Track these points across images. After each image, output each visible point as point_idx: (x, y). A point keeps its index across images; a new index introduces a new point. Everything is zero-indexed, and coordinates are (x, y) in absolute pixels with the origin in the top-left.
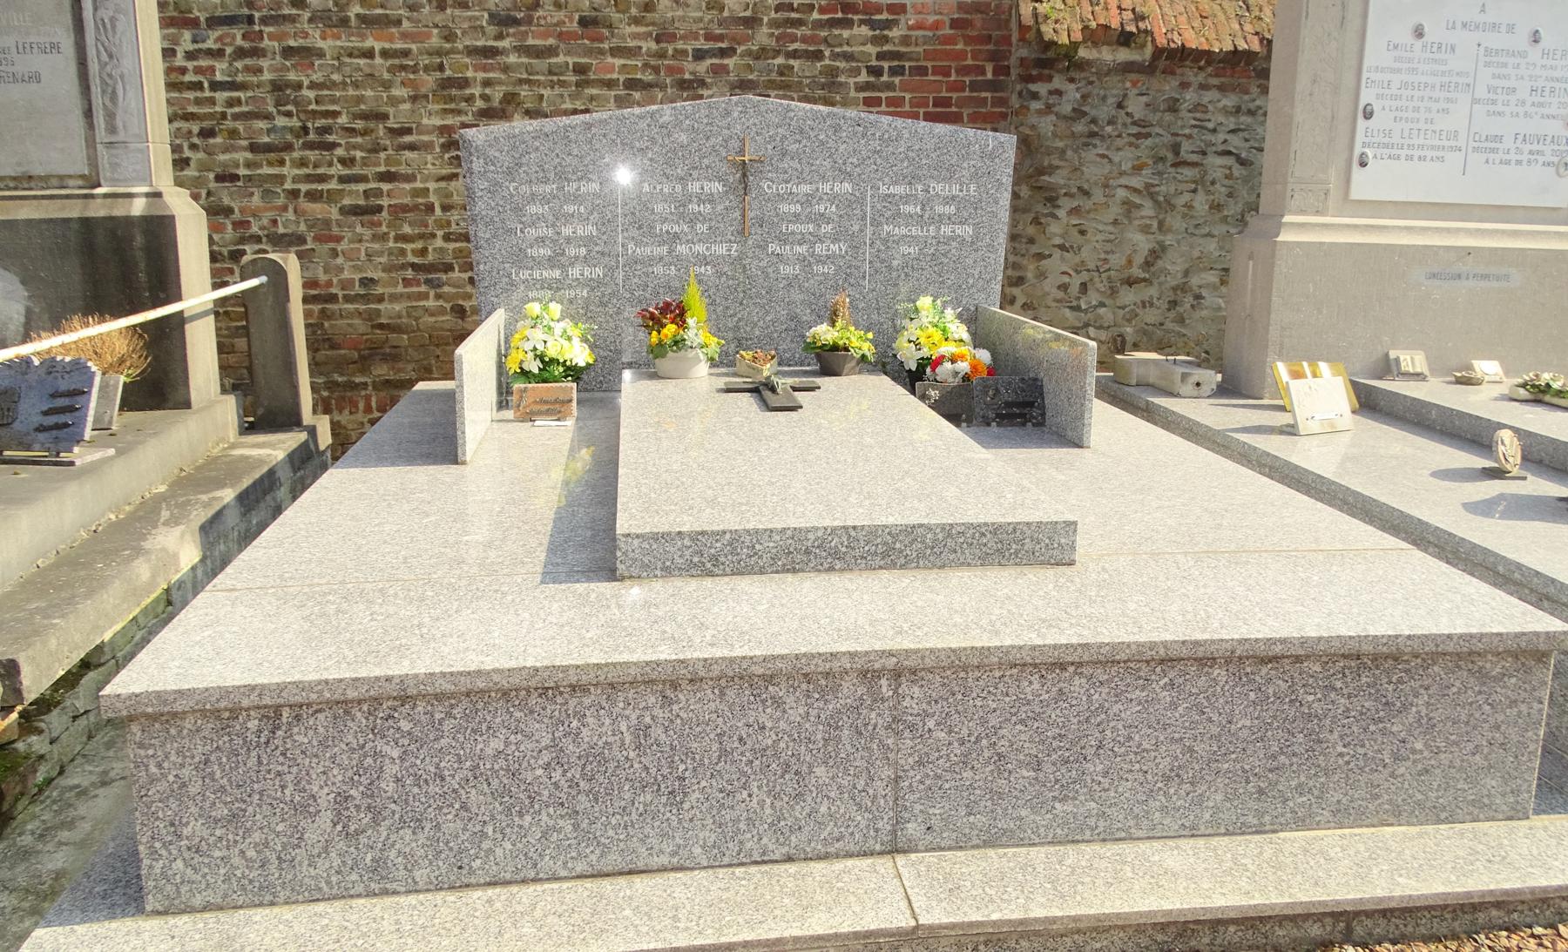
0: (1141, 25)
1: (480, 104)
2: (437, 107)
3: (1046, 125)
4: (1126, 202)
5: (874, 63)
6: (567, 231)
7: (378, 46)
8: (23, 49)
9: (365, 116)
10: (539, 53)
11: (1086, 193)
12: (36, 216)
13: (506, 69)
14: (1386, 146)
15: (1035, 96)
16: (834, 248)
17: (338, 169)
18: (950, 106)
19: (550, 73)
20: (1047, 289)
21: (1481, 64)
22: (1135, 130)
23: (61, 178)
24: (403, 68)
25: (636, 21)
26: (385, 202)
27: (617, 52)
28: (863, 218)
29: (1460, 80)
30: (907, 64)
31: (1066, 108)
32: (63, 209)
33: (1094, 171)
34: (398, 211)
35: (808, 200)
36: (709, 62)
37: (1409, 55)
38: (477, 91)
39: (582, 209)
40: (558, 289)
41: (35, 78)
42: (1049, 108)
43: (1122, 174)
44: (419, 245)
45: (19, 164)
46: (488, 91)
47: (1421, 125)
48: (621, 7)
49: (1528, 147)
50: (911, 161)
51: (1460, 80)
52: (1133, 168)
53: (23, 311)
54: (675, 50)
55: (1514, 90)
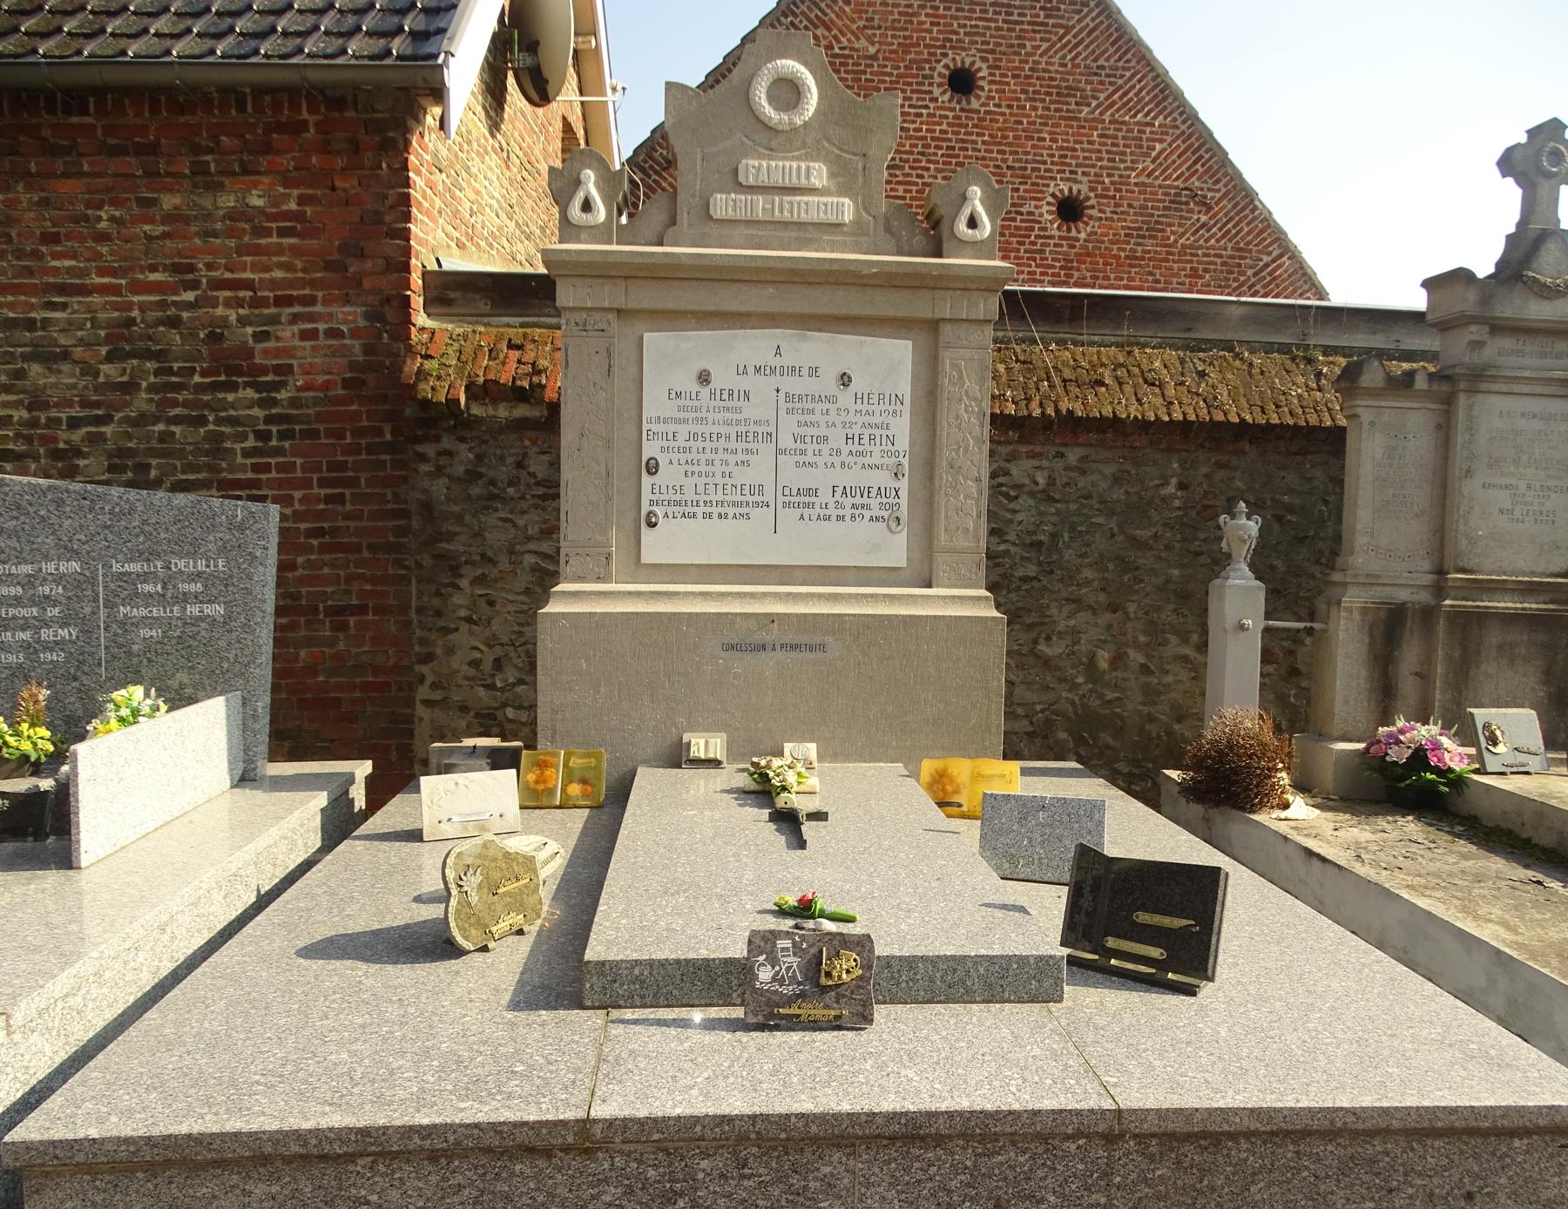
0: (535, 379)
3: (439, 488)
4: (535, 569)
5: (262, 427)
11: (492, 561)
14: (678, 503)
15: (423, 458)
16: (63, 633)
18: (346, 470)
20: (455, 665)
21: (782, 412)
22: (540, 491)
28: (96, 600)
29: (760, 429)
30: (297, 428)
31: (460, 470)
33: (497, 537)
35: (30, 582)
36: (84, 430)
37: (696, 403)
42: (440, 470)
43: (529, 539)
47: (719, 480)
49: (849, 501)
50: (148, 536)
51: (760, 429)
52: (542, 531)
54: (49, 419)
55: (826, 439)
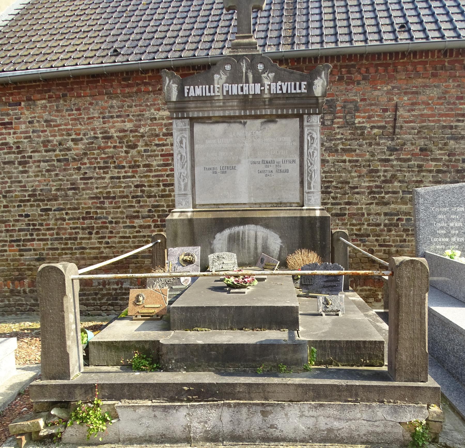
1: (382, 178)
2: (367, 179)
6: (452, 224)
7: (347, 159)
8: (284, 162)
9: (342, 183)
10: (405, 160)
12: (286, 216)
13: (392, 166)
17: (331, 201)
19: (409, 167)
23: (291, 203)
24: (356, 166)
25: (441, 149)
26: (347, 212)
27: (432, 160)
32: (294, 213)
34: (352, 215)
38: (381, 174)
39: (457, 217)
40: (447, 245)
41: (287, 171)
44: (358, 227)
45: (279, 199)
46: (385, 174)
48: (435, 144)
53: (279, 247)
54: (456, 159)
